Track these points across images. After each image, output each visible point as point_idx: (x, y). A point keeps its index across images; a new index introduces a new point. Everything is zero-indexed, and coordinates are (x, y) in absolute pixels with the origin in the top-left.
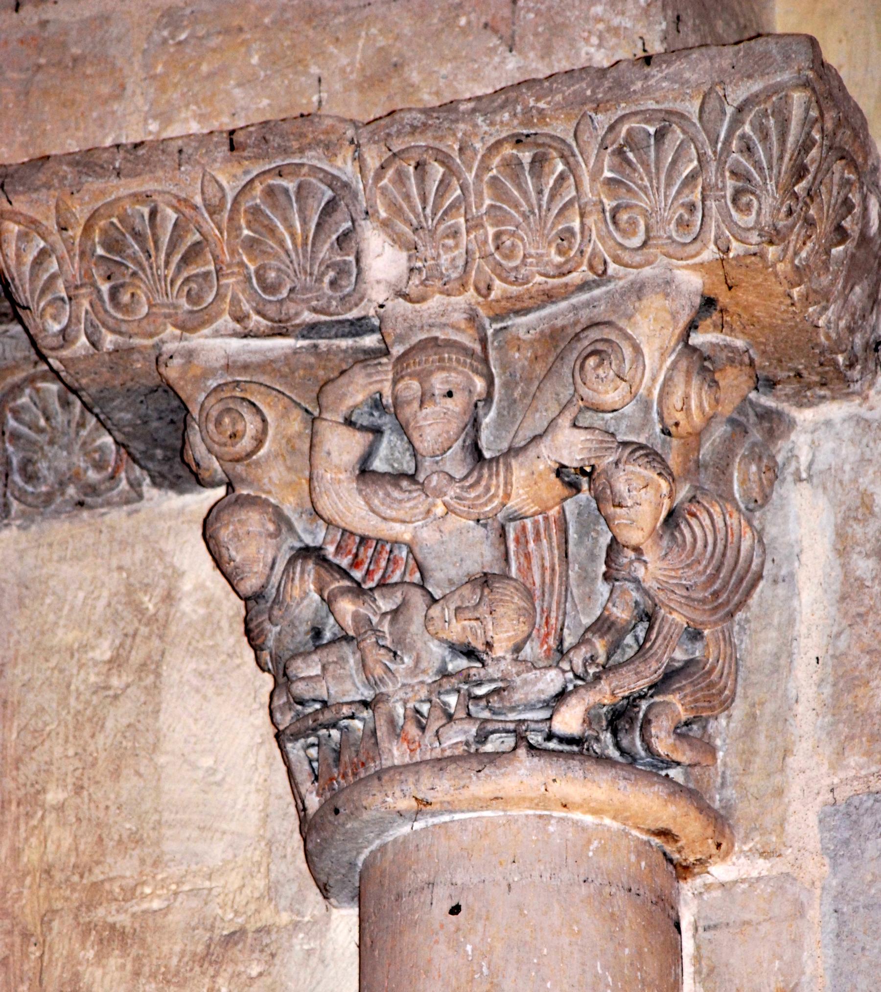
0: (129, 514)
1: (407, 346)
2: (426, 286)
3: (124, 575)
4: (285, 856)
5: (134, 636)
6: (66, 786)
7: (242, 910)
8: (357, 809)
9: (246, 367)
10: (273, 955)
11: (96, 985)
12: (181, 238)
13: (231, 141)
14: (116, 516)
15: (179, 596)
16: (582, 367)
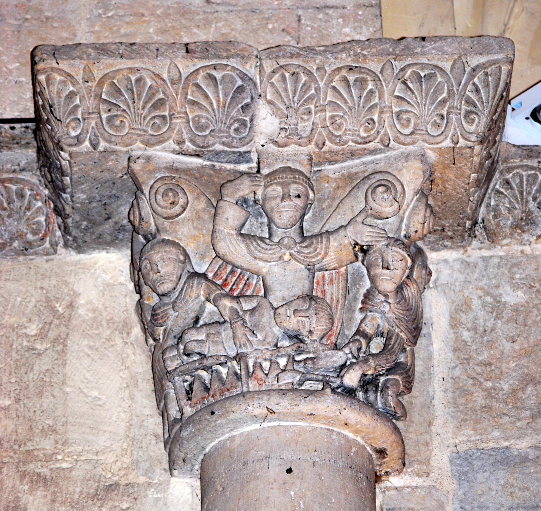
0: (47, 261)
1: (271, 170)
2: (289, 138)
3: (45, 292)
4: (142, 447)
5: (51, 324)
6: (10, 398)
7: (116, 473)
8: (227, 412)
9: (177, 170)
10: (136, 499)
11: (29, 504)
12: (154, 95)
13: (187, 48)
14: (40, 261)
15: (77, 306)
16: (374, 191)
